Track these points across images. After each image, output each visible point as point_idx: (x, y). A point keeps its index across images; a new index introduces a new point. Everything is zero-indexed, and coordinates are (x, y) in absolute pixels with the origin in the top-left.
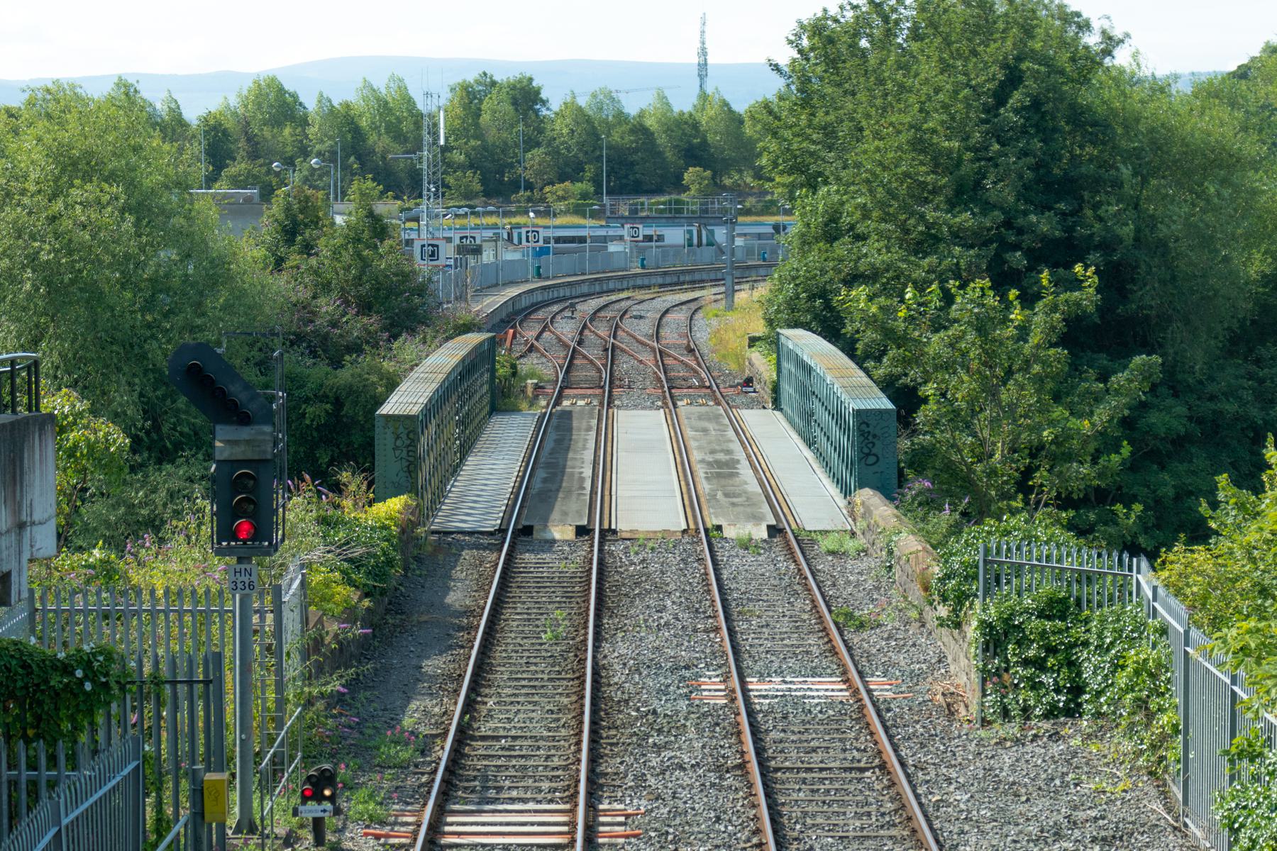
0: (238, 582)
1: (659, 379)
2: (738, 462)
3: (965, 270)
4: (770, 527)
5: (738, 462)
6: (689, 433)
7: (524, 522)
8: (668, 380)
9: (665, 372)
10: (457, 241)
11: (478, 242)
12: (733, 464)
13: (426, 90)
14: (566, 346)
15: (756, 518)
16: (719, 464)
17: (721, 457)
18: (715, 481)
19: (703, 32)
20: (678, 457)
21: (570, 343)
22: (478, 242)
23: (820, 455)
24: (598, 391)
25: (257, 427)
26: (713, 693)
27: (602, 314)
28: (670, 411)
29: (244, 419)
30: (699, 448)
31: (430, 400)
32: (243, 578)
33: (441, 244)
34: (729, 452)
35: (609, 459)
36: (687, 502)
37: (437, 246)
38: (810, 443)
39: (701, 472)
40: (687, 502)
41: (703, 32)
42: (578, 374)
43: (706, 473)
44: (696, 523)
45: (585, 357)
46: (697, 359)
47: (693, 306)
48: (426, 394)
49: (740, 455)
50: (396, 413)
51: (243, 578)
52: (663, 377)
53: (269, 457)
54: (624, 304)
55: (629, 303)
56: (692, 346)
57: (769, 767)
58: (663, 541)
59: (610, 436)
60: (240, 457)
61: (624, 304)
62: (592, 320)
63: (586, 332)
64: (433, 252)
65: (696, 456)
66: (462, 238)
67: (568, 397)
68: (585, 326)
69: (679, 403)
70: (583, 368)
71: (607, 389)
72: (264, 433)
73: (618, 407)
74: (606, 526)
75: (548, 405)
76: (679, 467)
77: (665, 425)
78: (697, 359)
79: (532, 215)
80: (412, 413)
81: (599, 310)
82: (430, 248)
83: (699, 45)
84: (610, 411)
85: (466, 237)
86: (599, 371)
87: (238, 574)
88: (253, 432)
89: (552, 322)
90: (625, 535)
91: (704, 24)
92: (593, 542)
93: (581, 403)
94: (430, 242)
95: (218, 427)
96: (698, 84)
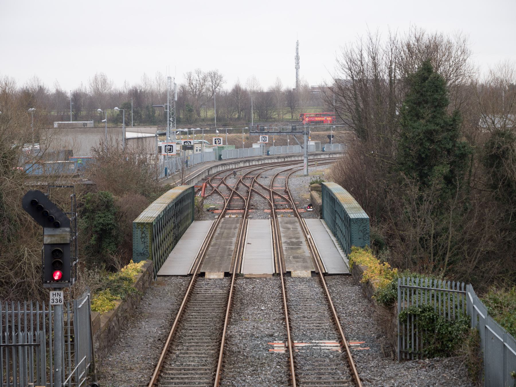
0: (55, 299)
1: (271, 206)
2: (301, 242)
3: (329, 156)
4: (312, 272)
5: (301, 242)
6: (281, 229)
7: (202, 271)
8: (275, 205)
9: (274, 202)
10: (183, 144)
11: (192, 144)
12: (299, 243)
13: (168, 76)
14: (230, 190)
15: (306, 268)
16: (292, 243)
17: (294, 240)
18: (290, 251)
19: (297, 49)
20: (274, 241)
21: (232, 189)
22: (192, 144)
23: (338, 240)
24: (242, 211)
25: (62, 229)
26: (408, 334)
27: (248, 176)
28: (274, 220)
29: (57, 225)
30: (284, 236)
31: (159, 215)
32: (57, 297)
33: (174, 145)
34: (298, 238)
35: (243, 242)
36: (276, 261)
37: (172, 146)
38: (335, 235)
39: (284, 247)
40: (276, 261)
41: (297, 49)
42: (234, 204)
43: (286, 248)
44: (279, 271)
45: (239, 195)
46: (289, 196)
47: (289, 172)
48: (157, 213)
49: (303, 239)
50: (142, 222)
51: (57, 297)
52: (272, 204)
53: (68, 242)
54: (258, 172)
55: (261, 171)
56: (287, 190)
57: (301, 381)
58: (263, 278)
59: (245, 232)
60: (55, 242)
61: (258, 172)
62: (243, 179)
63: (241, 184)
64: (170, 149)
65: (283, 240)
66: (185, 142)
67: (228, 214)
68: (240, 181)
69: (278, 216)
70: (237, 200)
71: (246, 209)
72: (66, 231)
73: (251, 218)
74: (238, 272)
75: (219, 217)
76: (275, 245)
77: (271, 226)
78: (289, 196)
79: (217, 132)
80: (149, 222)
81: (247, 174)
82: (169, 147)
83: (295, 54)
84: (247, 220)
85: (187, 142)
86: (244, 201)
87: (54, 296)
88: (61, 231)
89: (225, 180)
90: (246, 276)
91: (298, 45)
92: (232, 280)
93: (234, 216)
94: (168, 144)
95: (45, 229)
96: (295, 72)
